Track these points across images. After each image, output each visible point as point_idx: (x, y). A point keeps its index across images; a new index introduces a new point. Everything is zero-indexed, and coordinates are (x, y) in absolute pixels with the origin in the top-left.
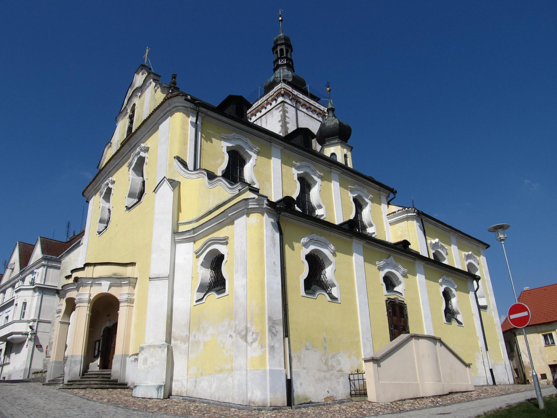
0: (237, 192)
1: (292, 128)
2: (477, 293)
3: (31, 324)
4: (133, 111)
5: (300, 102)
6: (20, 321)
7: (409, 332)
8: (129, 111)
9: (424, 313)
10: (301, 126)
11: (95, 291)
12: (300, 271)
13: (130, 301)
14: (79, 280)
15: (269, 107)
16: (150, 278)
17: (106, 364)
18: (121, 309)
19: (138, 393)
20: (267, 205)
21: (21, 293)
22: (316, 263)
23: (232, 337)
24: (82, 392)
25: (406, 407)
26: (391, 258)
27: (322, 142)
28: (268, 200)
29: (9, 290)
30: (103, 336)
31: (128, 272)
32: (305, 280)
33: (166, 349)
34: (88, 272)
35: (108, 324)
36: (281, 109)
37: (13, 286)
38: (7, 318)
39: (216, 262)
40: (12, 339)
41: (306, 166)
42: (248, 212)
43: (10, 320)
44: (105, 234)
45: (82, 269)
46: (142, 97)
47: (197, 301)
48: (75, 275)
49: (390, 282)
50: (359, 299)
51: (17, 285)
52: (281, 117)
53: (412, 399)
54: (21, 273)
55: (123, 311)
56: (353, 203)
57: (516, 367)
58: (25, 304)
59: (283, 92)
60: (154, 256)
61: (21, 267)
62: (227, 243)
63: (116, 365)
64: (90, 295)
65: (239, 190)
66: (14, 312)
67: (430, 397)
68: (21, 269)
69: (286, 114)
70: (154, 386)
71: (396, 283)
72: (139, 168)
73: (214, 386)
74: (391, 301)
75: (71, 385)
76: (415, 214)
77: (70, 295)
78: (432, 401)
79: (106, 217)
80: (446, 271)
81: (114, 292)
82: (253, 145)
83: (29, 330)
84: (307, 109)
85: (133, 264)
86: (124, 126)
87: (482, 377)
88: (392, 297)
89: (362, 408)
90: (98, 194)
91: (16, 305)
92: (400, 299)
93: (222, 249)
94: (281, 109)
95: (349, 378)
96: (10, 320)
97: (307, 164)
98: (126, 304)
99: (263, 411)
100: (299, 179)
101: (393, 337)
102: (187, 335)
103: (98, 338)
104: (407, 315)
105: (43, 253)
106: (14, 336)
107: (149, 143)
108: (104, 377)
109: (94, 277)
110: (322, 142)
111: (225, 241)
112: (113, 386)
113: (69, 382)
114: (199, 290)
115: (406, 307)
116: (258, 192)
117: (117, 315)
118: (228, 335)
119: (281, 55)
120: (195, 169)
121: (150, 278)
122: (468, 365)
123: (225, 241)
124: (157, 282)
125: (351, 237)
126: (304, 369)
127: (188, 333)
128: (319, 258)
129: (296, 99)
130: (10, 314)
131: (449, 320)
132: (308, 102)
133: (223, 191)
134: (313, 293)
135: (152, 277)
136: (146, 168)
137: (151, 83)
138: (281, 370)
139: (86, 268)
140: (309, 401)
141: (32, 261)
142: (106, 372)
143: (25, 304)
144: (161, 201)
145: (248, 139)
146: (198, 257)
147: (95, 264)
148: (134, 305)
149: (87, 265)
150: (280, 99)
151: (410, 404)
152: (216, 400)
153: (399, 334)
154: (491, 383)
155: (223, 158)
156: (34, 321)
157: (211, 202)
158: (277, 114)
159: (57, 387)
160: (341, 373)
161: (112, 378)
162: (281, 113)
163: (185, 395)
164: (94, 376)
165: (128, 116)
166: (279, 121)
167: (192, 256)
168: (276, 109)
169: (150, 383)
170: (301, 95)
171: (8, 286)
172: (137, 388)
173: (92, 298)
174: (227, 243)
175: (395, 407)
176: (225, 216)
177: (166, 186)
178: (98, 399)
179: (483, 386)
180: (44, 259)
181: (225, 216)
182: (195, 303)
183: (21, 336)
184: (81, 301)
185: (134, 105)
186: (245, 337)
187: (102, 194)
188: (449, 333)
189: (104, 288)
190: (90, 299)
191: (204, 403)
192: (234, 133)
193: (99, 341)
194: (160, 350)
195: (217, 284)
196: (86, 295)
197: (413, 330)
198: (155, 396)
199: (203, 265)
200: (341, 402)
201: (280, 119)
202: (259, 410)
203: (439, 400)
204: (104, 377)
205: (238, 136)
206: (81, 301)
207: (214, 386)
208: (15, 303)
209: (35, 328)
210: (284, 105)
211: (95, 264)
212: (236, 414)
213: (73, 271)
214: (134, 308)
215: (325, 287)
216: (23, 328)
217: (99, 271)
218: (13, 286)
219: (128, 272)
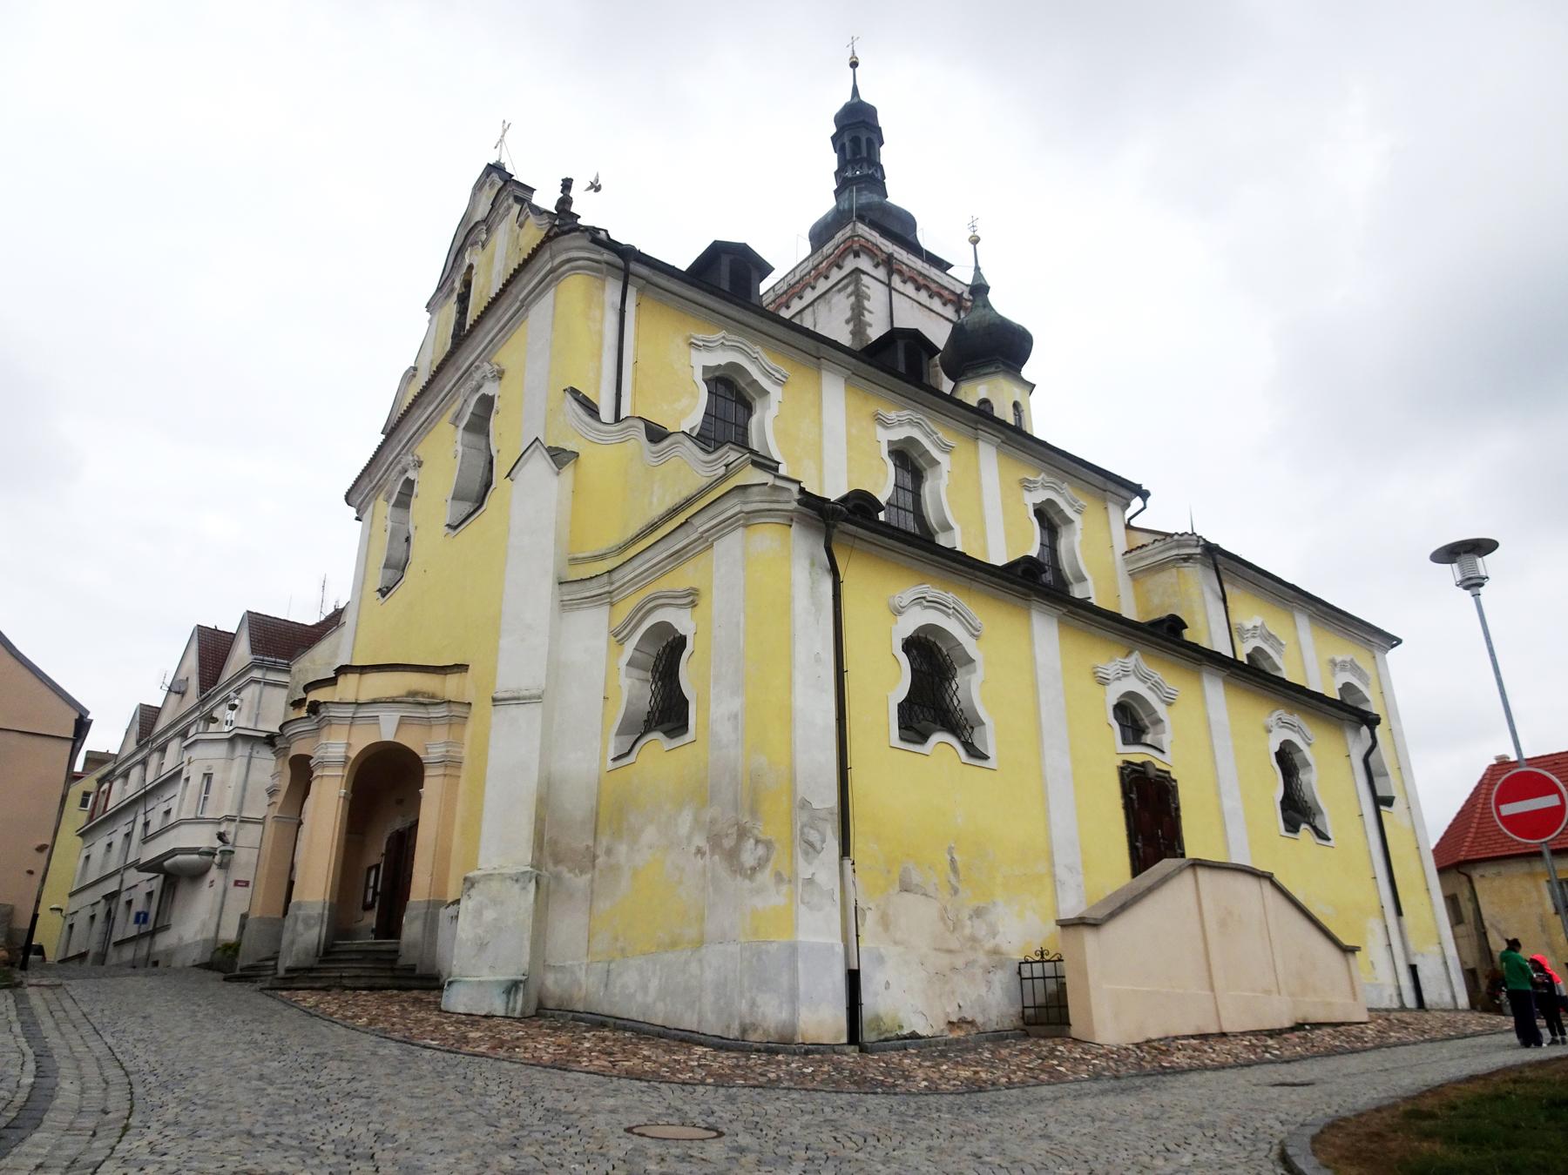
0: (722, 471)
1: (875, 332)
2: (1370, 742)
3: (222, 829)
4: (467, 284)
5: (900, 273)
6: (198, 821)
7: (1183, 855)
8: (457, 285)
9: (1226, 800)
10: (902, 322)
11: (363, 739)
12: (885, 681)
13: (451, 764)
14: (322, 710)
15: (822, 285)
16: (494, 700)
17: (390, 925)
18: (427, 782)
19: (457, 1000)
20: (799, 502)
21: (197, 752)
22: (931, 660)
23: (703, 854)
24: (312, 999)
25: (1180, 1059)
26: (1136, 655)
27: (957, 373)
28: (802, 490)
29: (174, 747)
30: (387, 854)
31: (450, 686)
32: (900, 705)
33: (533, 885)
34: (349, 688)
35: (398, 824)
36: (850, 289)
37: (184, 735)
38: (167, 813)
39: (667, 655)
40: (176, 866)
41: (911, 423)
42: (748, 519)
43: (173, 818)
44: (399, 593)
45: (332, 682)
46: (489, 247)
47: (614, 760)
48: (313, 696)
49: (1132, 719)
50: (1057, 760)
51: (192, 731)
52: (853, 309)
53: (1193, 1037)
54: (203, 702)
55: (432, 788)
56: (1035, 520)
57: (1471, 965)
58: (208, 777)
59: (856, 246)
60: (504, 643)
61: (203, 689)
62: (693, 604)
63: (412, 929)
64: (349, 745)
65: (727, 466)
66: (182, 800)
67: (1244, 1034)
68: (202, 692)
69: (866, 303)
70: (498, 983)
71: (1147, 722)
72: (480, 421)
73: (654, 984)
74: (1134, 771)
75: (292, 979)
76: (1198, 550)
77: (297, 749)
78: (1252, 1045)
79: (399, 555)
80: (1287, 697)
81: (411, 739)
82: (774, 365)
83: (217, 844)
84: (918, 289)
85: (462, 668)
86: (447, 324)
87: (1379, 981)
88: (1138, 759)
89: (1056, 1057)
90: (382, 496)
91: (187, 779)
92: (1159, 765)
93: (682, 621)
94: (850, 289)
95: (1019, 973)
96: (173, 818)
97: (916, 416)
98: (441, 771)
99: (780, 1057)
100: (891, 453)
101: (1140, 863)
102: (588, 847)
103: (375, 862)
104: (1177, 809)
105: (253, 651)
106: (179, 858)
107: (506, 356)
108: (378, 959)
109: (362, 699)
110: (956, 376)
111: (691, 598)
112: (402, 983)
113: (288, 970)
114: (621, 732)
115: (1175, 788)
116: (777, 469)
117: (419, 798)
118: (693, 850)
119: (854, 153)
120: (617, 419)
121: (494, 700)
122: (1348, 951)
123: (691, 598)
124: (513, 711)
125: (1025, 597)
126: (896, 943)
127: (591, 843)
128: (940, 650)
129: (889, 263)
130: (174, 804)
131: (1292, 826)
132: (920, 274)
133: (689, 470)
134: (922, 738)
135: (500, 695)
136: (495, 423)
137: (509, 208)
138: (832, 946)
139: (341, 679)
140: (905, 1032)
141: (229, 672)
142: (387, 944)
143: (208, 777)
144: (531, 503)
145: (758, 348)
146: (621, 642)
147: (363, 670)
148: (463, 774)
149: (343, 670)
150: (850, 263)
151: (1190, 1052)
152: (659, 1022)
153: (1158, 859)
154: (1410, 1001)
155: (695, 396)
156: (230, 819)
157: (655, 500)
158: (842, 304)
159: (259, 985)
160: (996, 957)
161: (401, 962)
162: (852, 299)
163: (580, 1007)
164: (354, 956)
165: (454, 297)
166: (848, 322)
167: (602, 641)
168: (839, 291)
169: (487, 976)
170: (904, 253)
171: (170, 733)
172: (455, 987)
173: (353, 755)
174: (693, 604)
175: (1148, 1058)
176: (680, 528)
177: (539, 465)
178: (345, 1018)
179: (1387, 1010)
180: (253, 666)
181: (680, 528)
182: (610, 765)
183: (196, 857)
184: (323, 764)
185: (471, 267)
186: (732, 856)
187: (390, 497)
188: (1295, 858)
189: (387, 728)
190: (347, 758)
191: (625, 1029)
192: (723, 333)
193: (377, 867)
194: (517, 887)
195: (668, 712)
196: (338, 747)
197: (1193, 849)
198: (499, 1007)
199: (631, 663)
200: (998, 1037)
201: (848, 314)
202: (772, 1052)
203: (1270, 1042)
204: (378, 959)
205: (734, 339)
206: (323, 764)
207: (654, 984)
208: (184, 776)
209: (230, 838)
210: (858, 282)
211: (363, 670)
212: (703, 1062)
213: (308, 688)
214: (462, 781)
215: (960, 725)
216: (202, 838)
217: (376, 685)
218: (184, 735)
219: (450, 686)
